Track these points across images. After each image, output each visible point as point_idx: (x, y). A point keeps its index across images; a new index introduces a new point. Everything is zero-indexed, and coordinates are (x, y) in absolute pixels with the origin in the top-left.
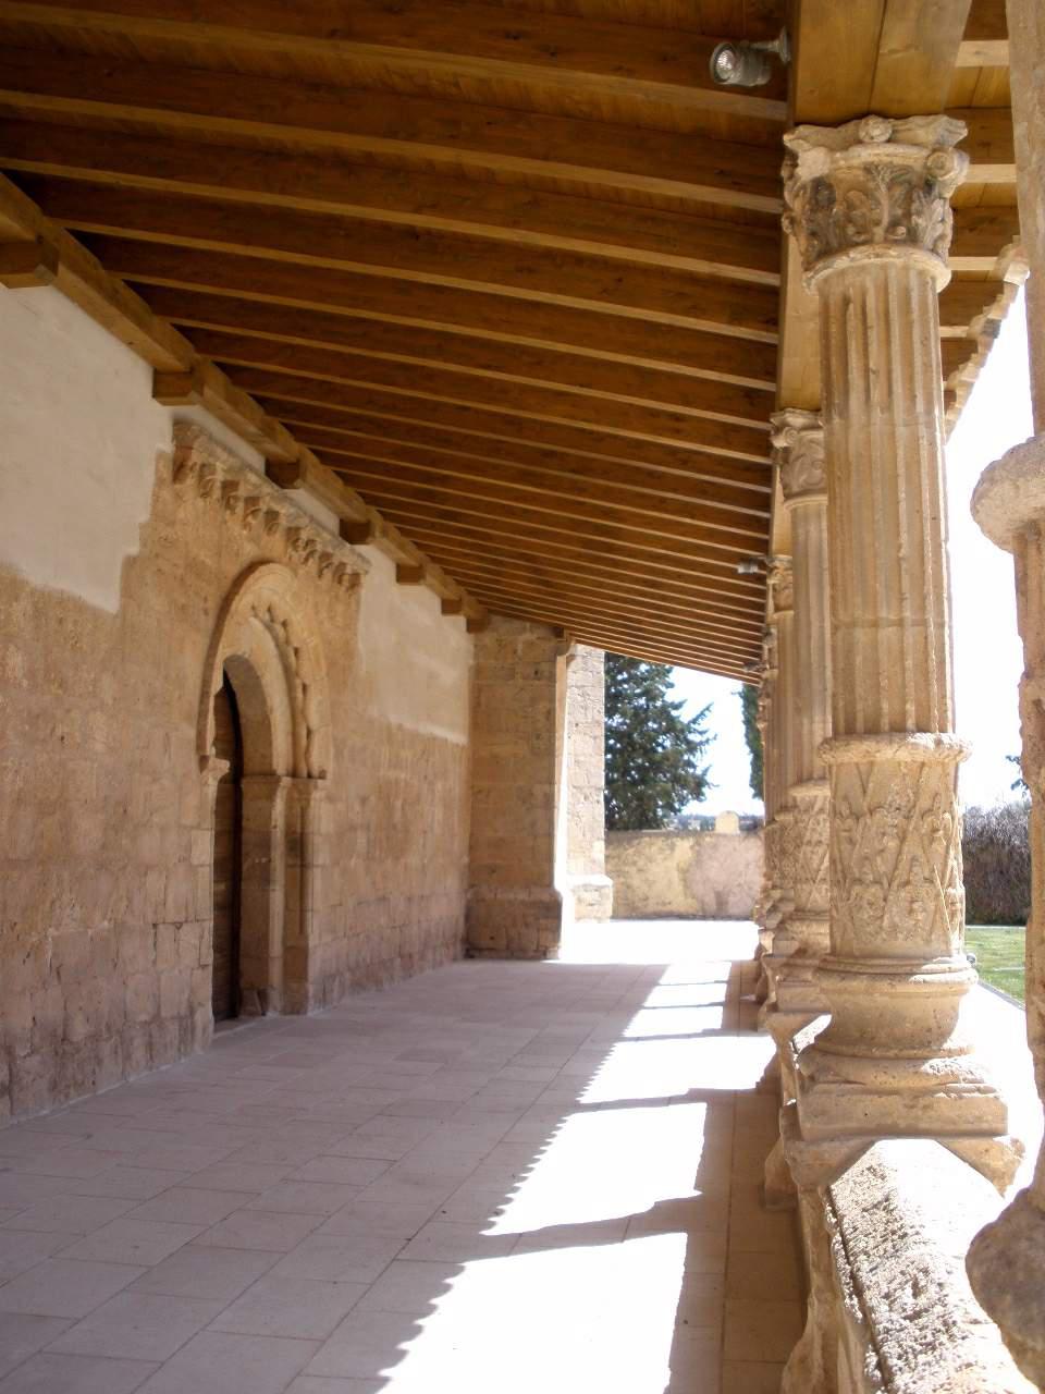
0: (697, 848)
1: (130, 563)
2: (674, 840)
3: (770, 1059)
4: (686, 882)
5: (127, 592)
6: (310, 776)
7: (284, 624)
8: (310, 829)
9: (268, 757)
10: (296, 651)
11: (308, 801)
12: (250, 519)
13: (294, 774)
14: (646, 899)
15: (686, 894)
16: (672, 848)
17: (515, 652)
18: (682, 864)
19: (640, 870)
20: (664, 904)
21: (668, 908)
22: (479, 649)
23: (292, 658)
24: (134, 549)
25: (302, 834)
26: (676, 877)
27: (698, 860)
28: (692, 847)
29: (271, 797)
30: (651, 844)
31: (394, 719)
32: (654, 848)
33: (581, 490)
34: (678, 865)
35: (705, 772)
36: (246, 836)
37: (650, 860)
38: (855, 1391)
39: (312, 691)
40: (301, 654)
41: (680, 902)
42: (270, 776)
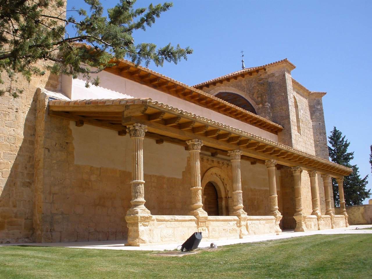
0: (365, 208)
1: (184, 172)
2: (360, 207)
3: (191, 235)
4: (363, 217)
5: (183, 175)
6: (229, 198)
7: (220, 175)
8: (229, 206)
9: (221, 195)
10: (223, 179)
11: (228, 201)
12: (208, 162)
13: (226, 198)
14: (355, 221)
15: (363, 220)
16: (359, 209)
17: (288, 172)
18: (362, 213)
19: (353, 214)
20: (359, 222)
21: (360, 223)
22: (281, 172)
23: (223, 180)
24: (184, 170)
25: (228, 206)
26: (361, 215)
27: (365, 211)
28: (364, 208)
29: (222, 201)
30: (354, 208)
31: (252, 187)
32: (355, 209)
33: (138, 144)
34: (361, 212)
35: (369, 191)
36: (219, 208)
37: (355, 212)
38: (1, 255)
39: (227, 185)
40: (224, 179)
41: (362, 221)
42: (221, 198)
